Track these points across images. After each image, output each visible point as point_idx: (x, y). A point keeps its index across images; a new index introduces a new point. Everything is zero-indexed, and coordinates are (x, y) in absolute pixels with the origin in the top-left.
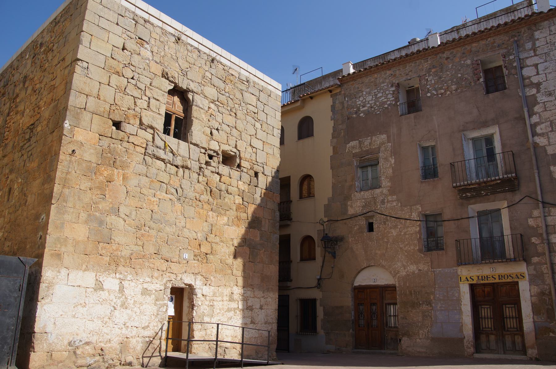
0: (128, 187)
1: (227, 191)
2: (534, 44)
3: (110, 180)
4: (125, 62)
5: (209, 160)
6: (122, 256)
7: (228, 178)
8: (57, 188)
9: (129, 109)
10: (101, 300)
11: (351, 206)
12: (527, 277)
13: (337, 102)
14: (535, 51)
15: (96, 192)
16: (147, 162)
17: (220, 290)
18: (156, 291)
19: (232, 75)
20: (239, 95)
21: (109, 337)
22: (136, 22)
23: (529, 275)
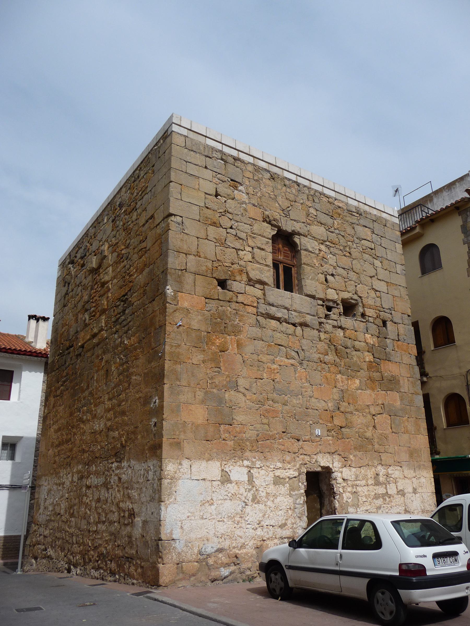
0: (243, 355)
3: (223, 349)
4: (220, 211)
6: (247, 440)
7: (353, 332)
9: (233, 264)
15: (209, 365)
16: (261, 324)
18: (290, 478)
19: (340, 207)
20: (349, 230)
21: (242, 541)
22: (225, 162)
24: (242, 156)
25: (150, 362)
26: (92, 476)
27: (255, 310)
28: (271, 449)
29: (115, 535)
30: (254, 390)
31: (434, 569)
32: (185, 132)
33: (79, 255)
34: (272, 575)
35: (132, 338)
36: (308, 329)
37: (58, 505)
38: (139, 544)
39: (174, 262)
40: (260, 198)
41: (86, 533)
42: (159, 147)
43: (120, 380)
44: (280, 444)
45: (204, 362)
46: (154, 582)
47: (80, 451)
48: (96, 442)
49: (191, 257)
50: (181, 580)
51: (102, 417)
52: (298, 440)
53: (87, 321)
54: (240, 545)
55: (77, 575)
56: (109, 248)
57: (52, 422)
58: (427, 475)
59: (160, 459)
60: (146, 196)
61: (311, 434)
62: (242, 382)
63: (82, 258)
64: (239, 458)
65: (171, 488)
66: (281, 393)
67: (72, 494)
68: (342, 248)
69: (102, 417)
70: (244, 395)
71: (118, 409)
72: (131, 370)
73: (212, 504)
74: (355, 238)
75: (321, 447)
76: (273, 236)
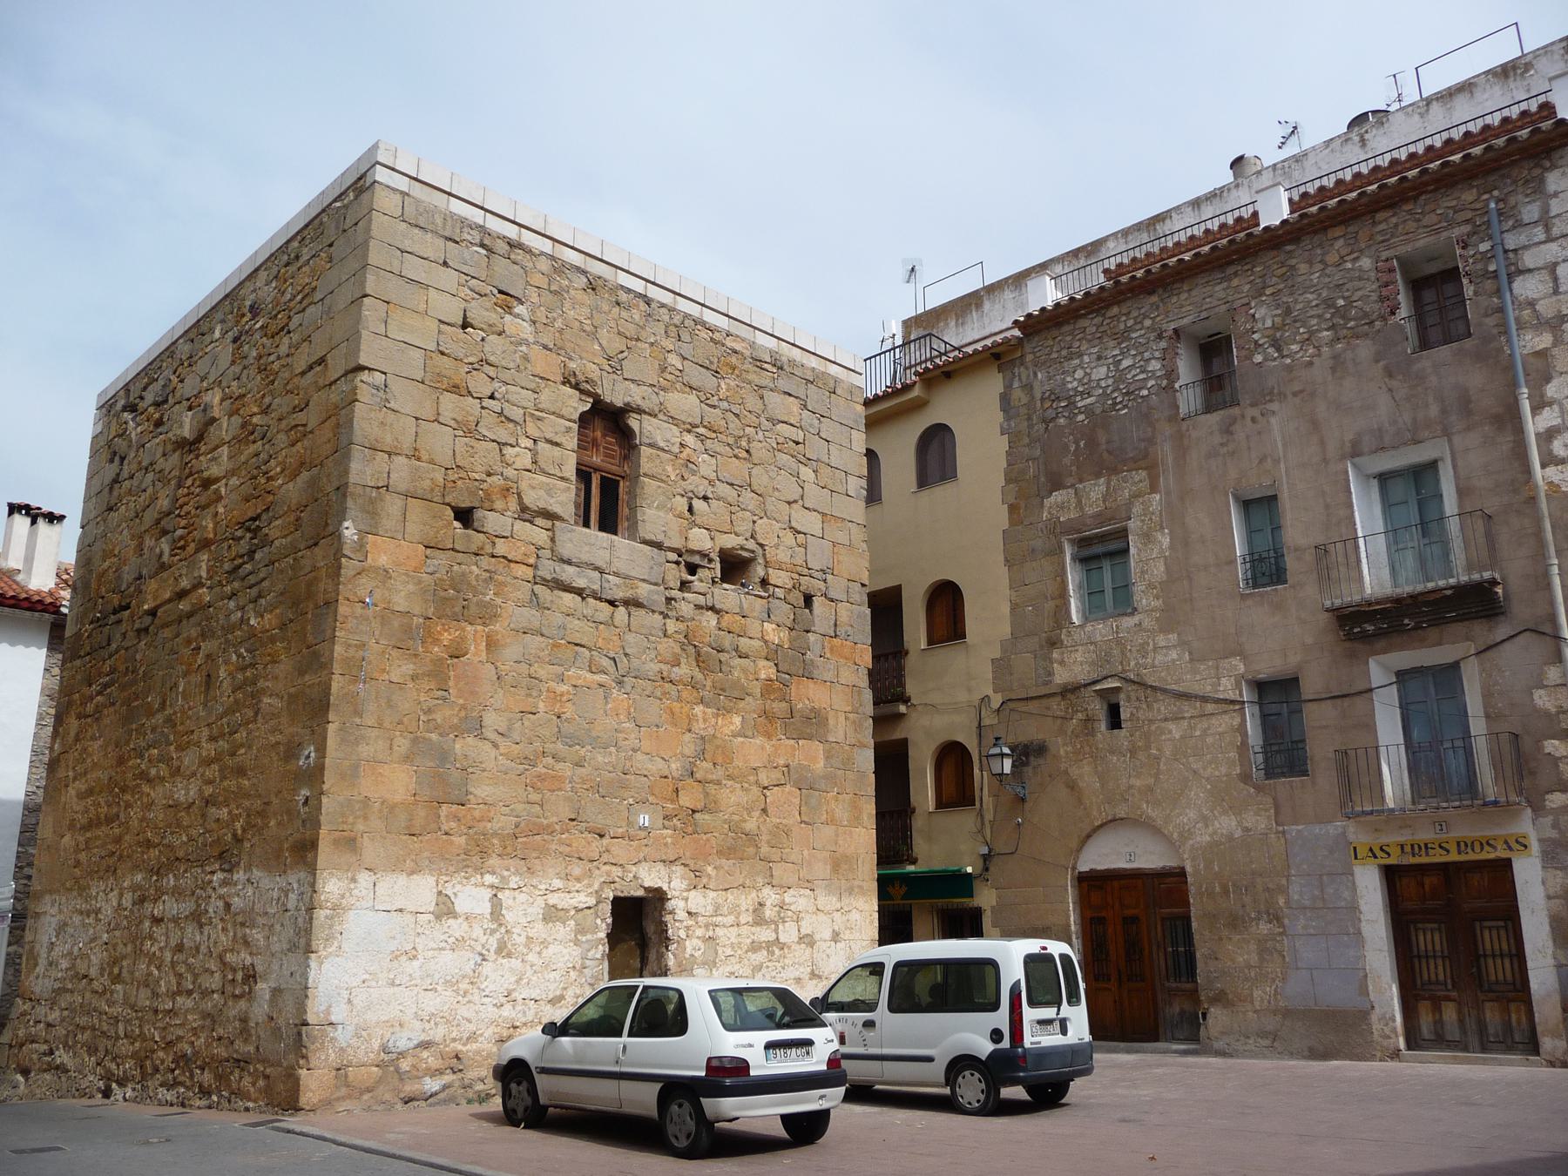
1: (736, 650)
2: (1546, 210)
4: (471, 359)
5: (690, 578)
6: (495, 834)
8: (337, 684)
9: (489, 475)
10: (451, 940)
11: (1062, 663)
12: (1535, 847)
13: (1016, 384)
14: (1547, 228)
17: (731, 897)
18: (578, 910)
20: (752, 402)
21: (472, 1027)
22: (490, 250)
23: (1540, 840)
24: (529, 239)
25: (302, 673)
26: (165, 897)
27: (529, 572)
28: (543, 852)
29: (212, 1018)
30: (516, 736)
31: (762, 1066)
32: (403, 184)
33: (149, 397)
34: (513, 1086)
35: (267, 616)
36: (642, 612)
37: (84, 956)
38: (262, 1034)
39: (362, 470)
40: (561, 331)
41: (149, 1016)
42: (345, 207)
43: (236, 701)
44: (561, 843)
45: (414, 678)
46: (292, 1104)
47: (139, 844)
48: (179, 825)
49: (401, 460)
50: (343, 1098)
51: (194, 774)
52: (601, 836)
53: (165, 558)
54: (466, 1035)
55: (125, 1099)
56: (222, 400)
57: (71, 774)
58: (866, 907)
59: (312, 869)
60: (311, 309)
61: (630, 824)
62: (492, 720)
63: (157, 404)
64: (476, 869)
65: (331, 927)
66: (573, 741)
67: (117, 933)
68: (731, 440)
69: (194, 774)
70: (496, 746)
71: (229, 762)
72: (261, 684)
73: (415, 957)
74: (763, 420)
75: (647, 850)
76: (583, 415)
